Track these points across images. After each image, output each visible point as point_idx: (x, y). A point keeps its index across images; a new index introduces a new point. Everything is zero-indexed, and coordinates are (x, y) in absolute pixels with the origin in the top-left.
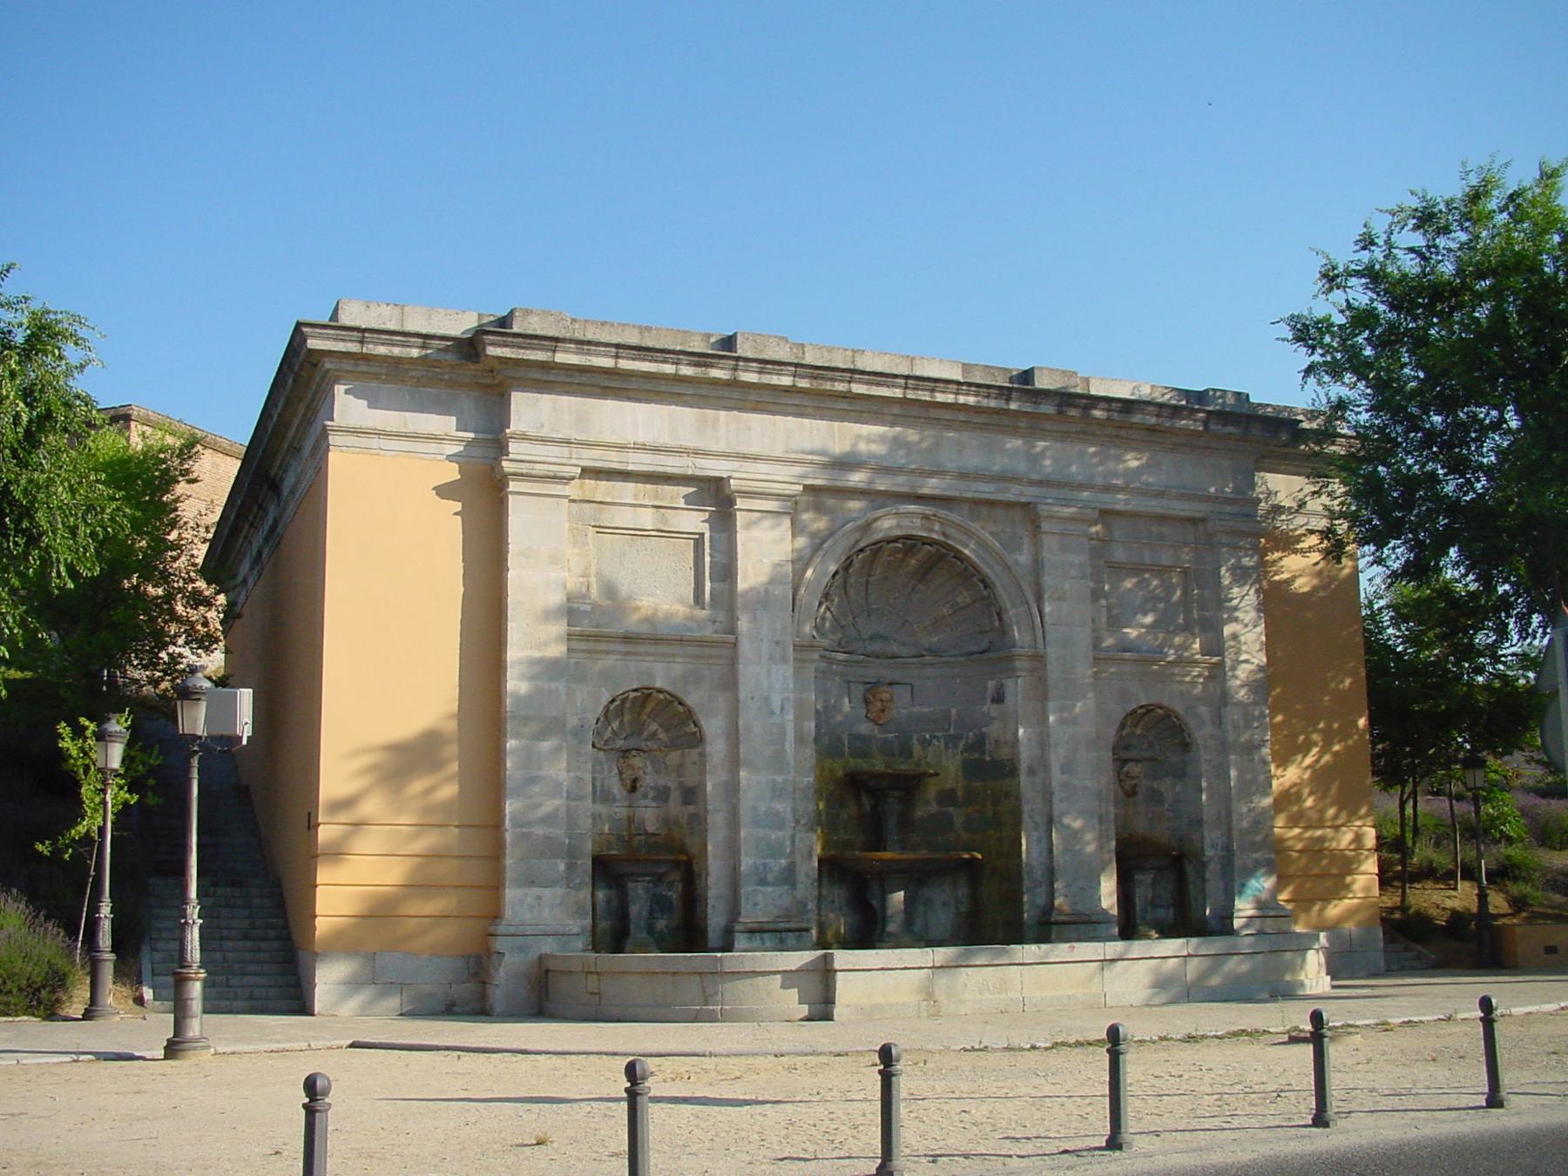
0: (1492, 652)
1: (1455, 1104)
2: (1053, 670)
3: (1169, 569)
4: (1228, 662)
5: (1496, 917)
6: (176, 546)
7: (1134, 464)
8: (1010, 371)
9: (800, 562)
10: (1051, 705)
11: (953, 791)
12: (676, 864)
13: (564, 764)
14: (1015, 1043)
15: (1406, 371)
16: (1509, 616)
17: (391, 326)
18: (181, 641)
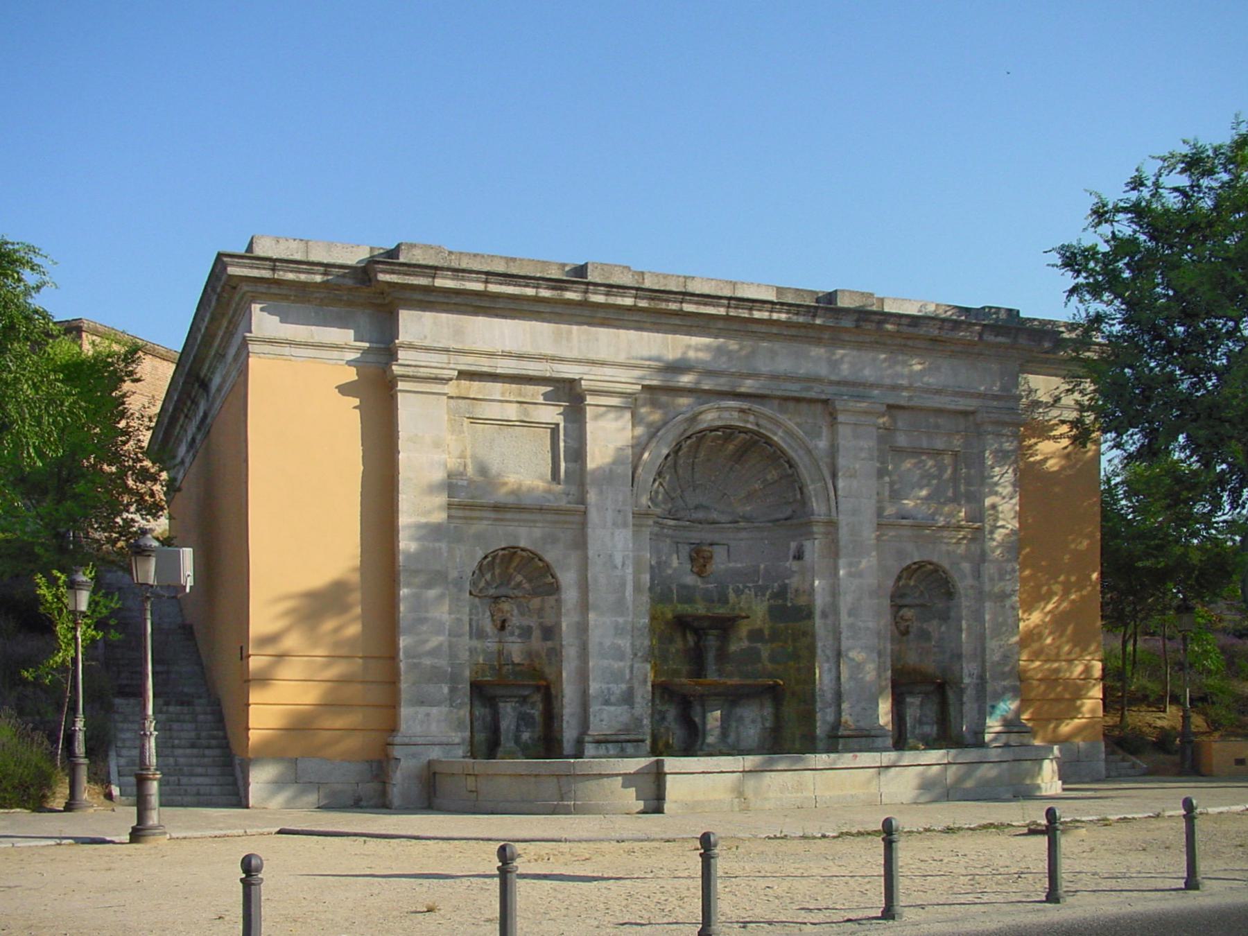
0: (1207, 519)
1: (1160, 885)
2: (844, 534)
3: (939, 453)
4: (987, 527)
5: (1196, 734)
6: (124, 432)
7: (919, 367)
8: (816, 293)
9: (639, 447)
10: (842, 562)
11: (761, 631)
12: (538, 688)
13: (446, 608)
14: (809, 832)
15: (1158, 290)
16: (1223, 490)
17: (298, 257)
18: (132, 509)
